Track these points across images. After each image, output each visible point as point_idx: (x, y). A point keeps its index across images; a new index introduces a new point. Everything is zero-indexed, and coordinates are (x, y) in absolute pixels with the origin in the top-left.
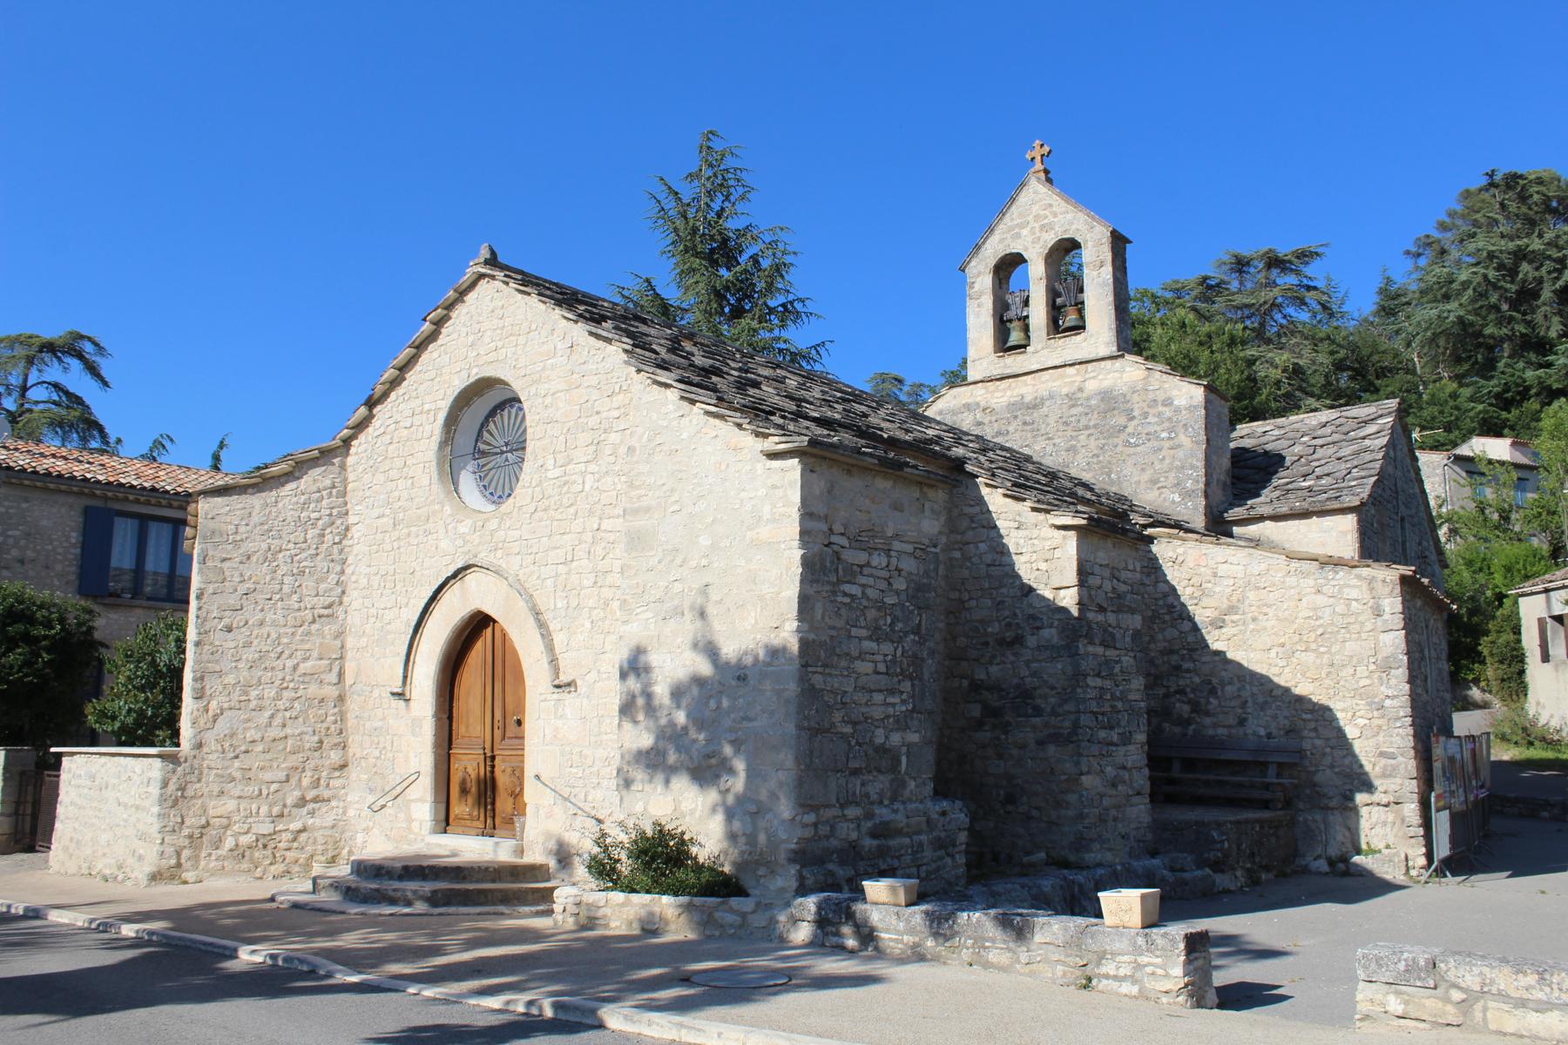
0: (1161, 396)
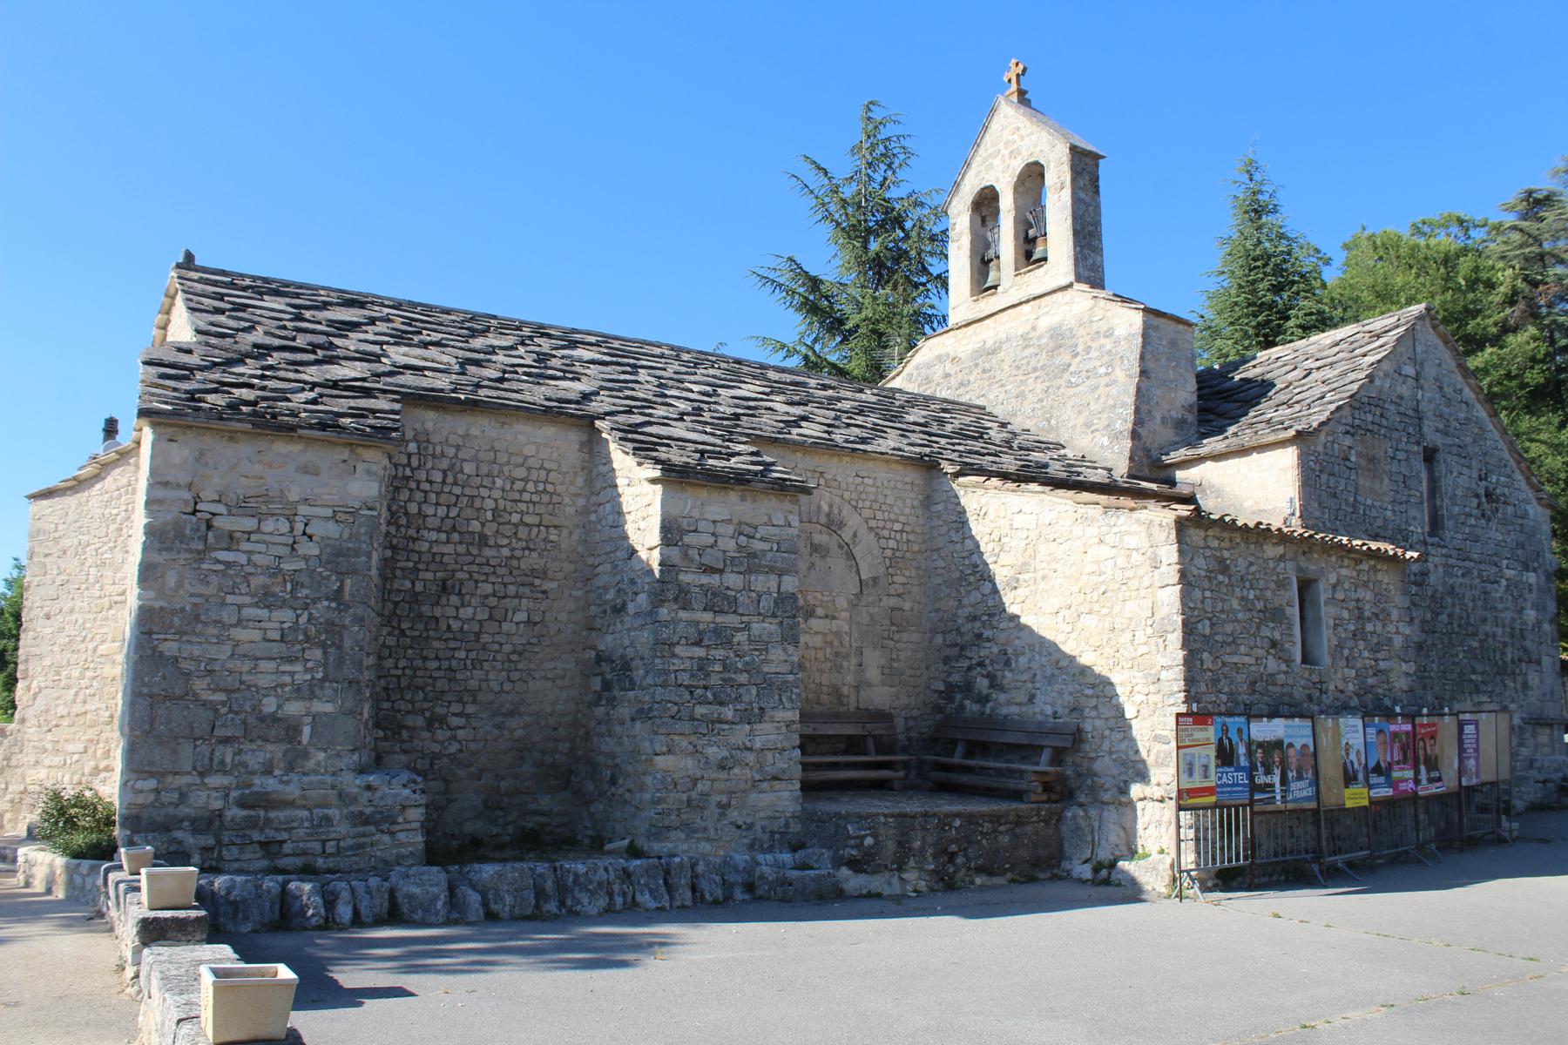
0: (1103, 326)
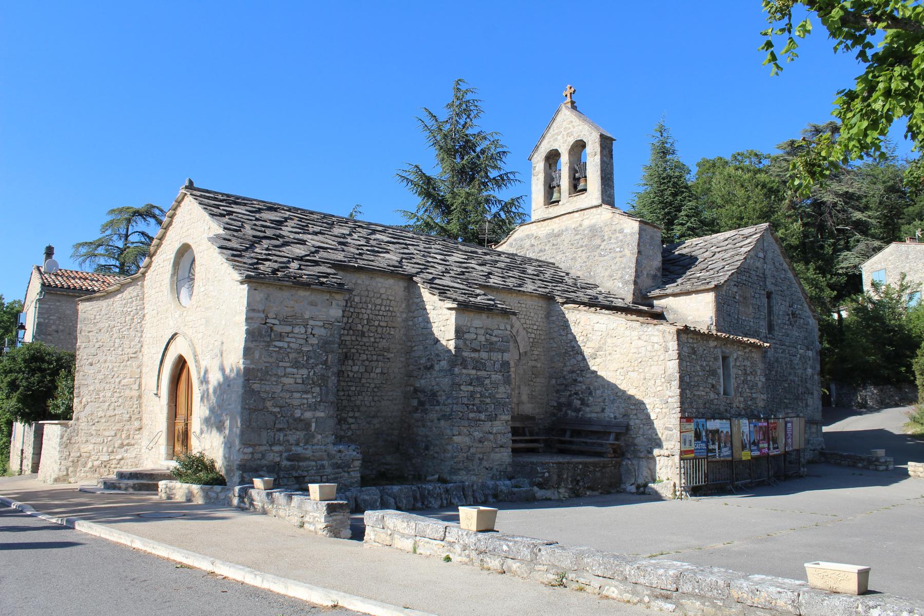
0: (618, 227)
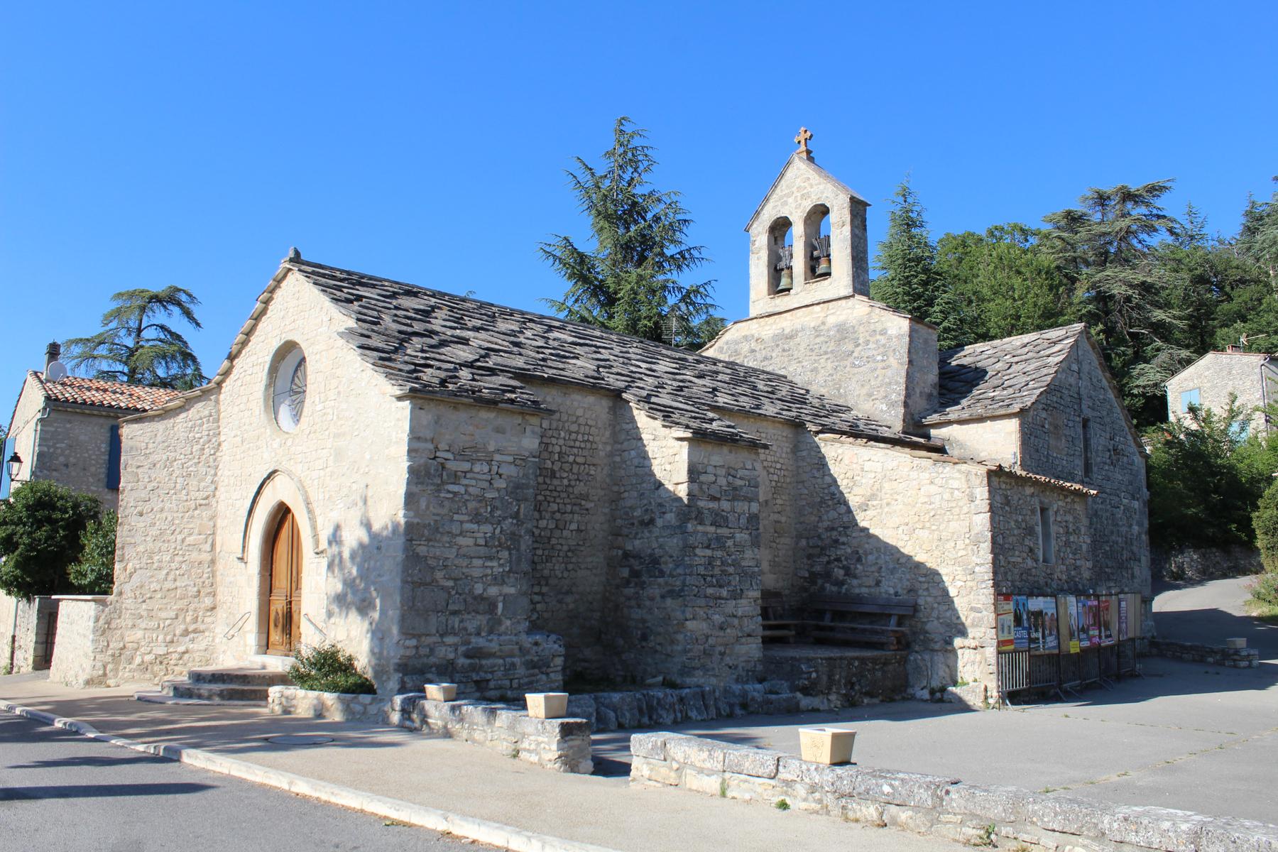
0: (879, 327)
